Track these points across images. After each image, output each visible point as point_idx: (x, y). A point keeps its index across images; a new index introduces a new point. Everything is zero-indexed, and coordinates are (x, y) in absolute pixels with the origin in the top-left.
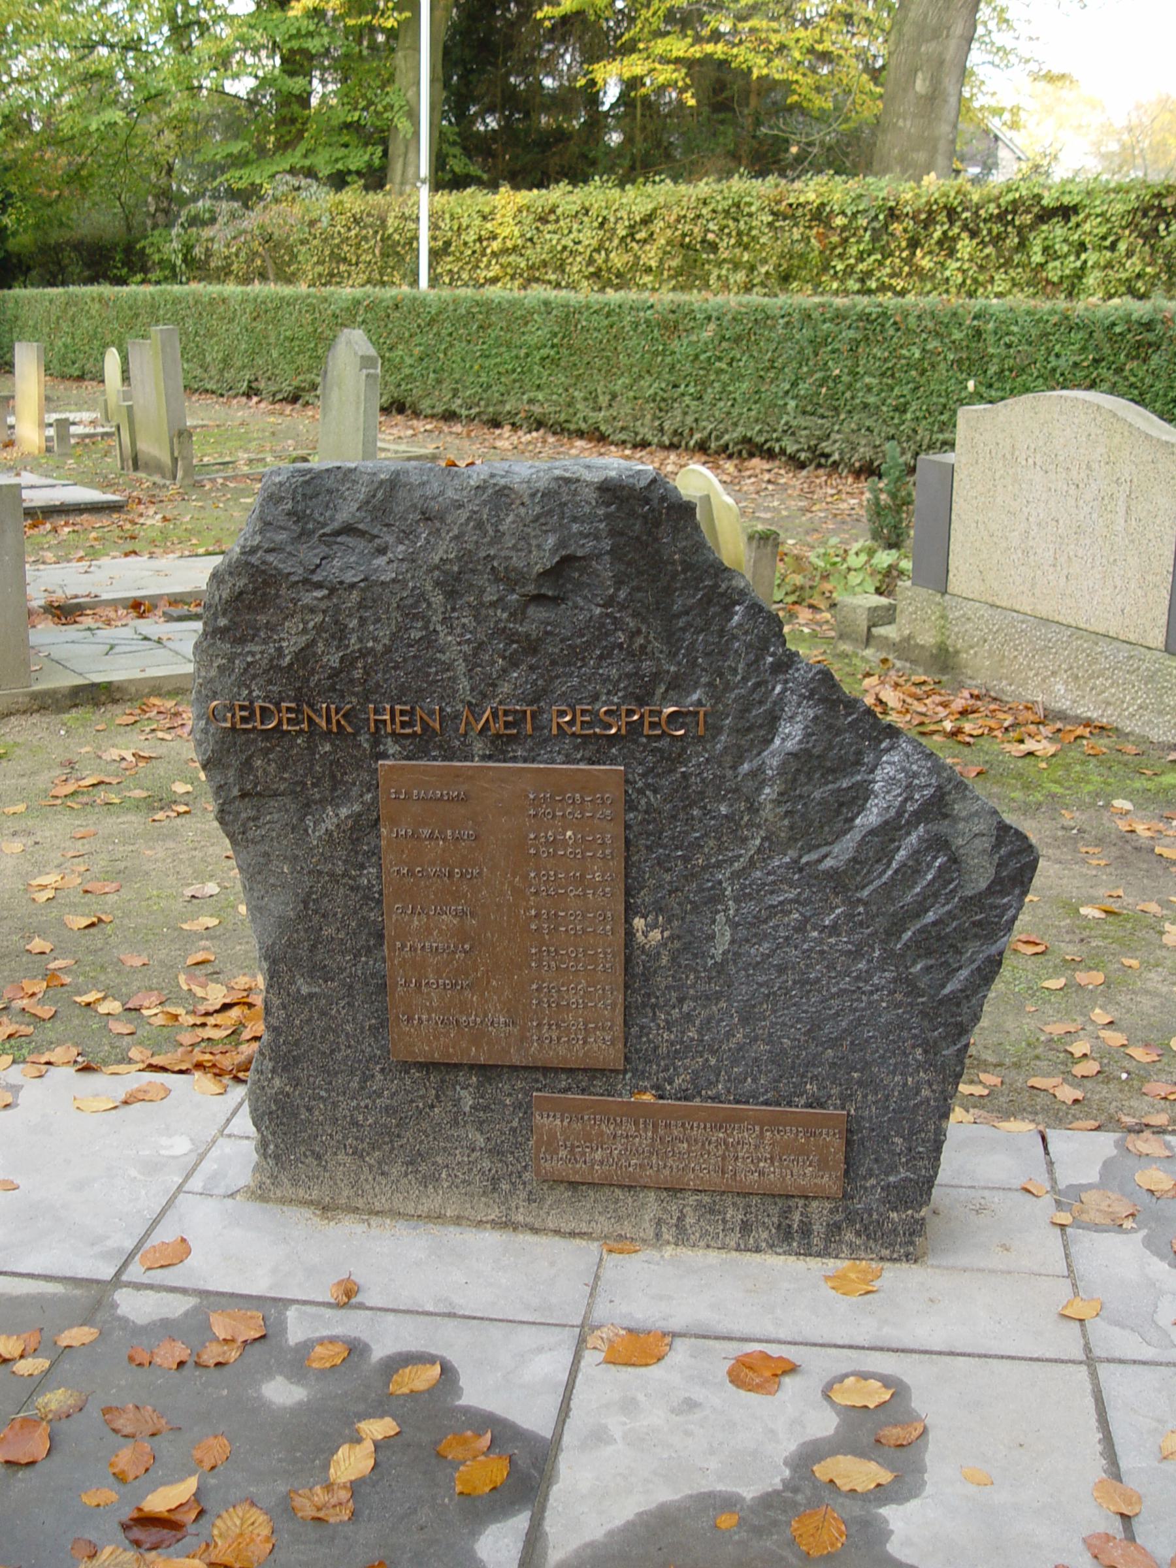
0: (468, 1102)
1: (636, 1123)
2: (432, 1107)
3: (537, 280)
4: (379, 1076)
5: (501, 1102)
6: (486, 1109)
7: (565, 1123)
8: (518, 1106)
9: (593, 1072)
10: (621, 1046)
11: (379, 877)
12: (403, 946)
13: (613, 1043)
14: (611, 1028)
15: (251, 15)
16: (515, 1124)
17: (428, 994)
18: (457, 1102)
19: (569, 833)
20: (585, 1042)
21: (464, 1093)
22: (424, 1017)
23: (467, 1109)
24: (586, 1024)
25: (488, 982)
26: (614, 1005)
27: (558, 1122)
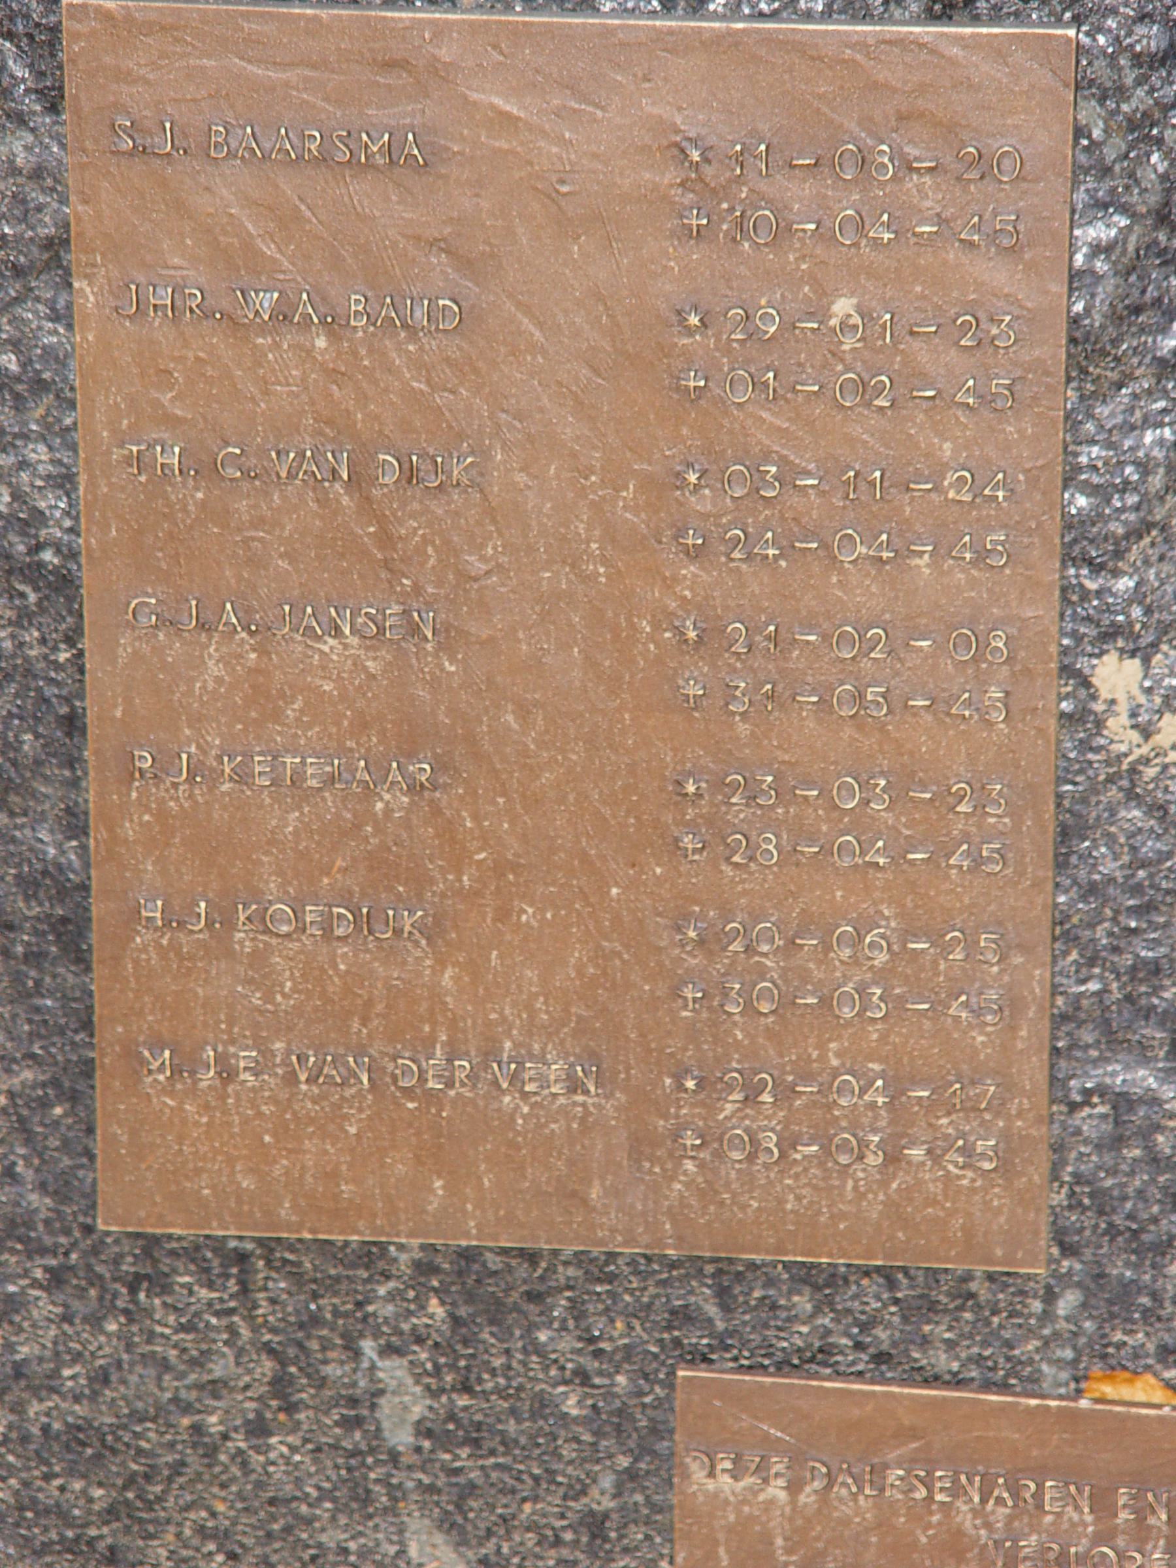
0: (404, 1404)
1: (1102, 1504)
2: (258, 1429)
3: (45, 440)
4: (44, 1306)
5: (543, 1406)
6: (474, 1438)
7: (807, 1497)
8: (613, 1421)
9: (928, 1295)
10: (1037, 1174)
11: (64, 481)
12: (164, 763)
13: (1006, 1167)
14: (998, 1107)
15: (833, 302)
16: (601, 1498)
17: (259, 958)
18: (357, 1410)
19: (843, 306)
20: (893, 1158)
21: (392, 1371)
22: (246, 1056)
23: (402, 1438)
24: (897, 1089)
25: (503, 914)
26: (1012, 1005)
27: (777, 1491)
